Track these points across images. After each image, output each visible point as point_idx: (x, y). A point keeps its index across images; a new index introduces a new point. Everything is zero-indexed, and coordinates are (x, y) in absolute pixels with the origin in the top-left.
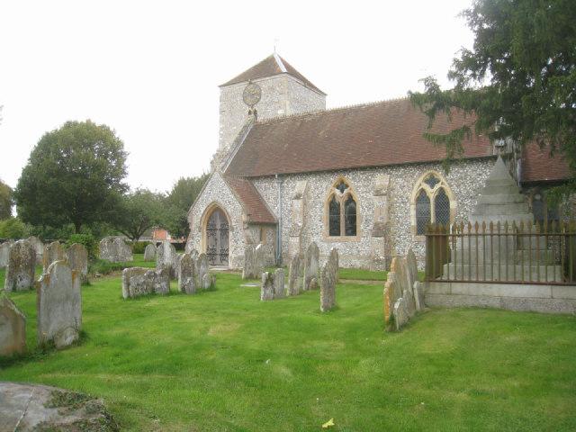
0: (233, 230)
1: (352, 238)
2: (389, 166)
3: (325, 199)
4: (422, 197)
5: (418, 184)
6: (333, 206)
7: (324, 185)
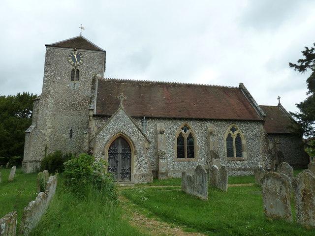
0: (136, 153)
1: (193, 159)
2: (249, 121)
3: (176, 135)
4: (229, 138)
5: (227, 131)
6: (180, 139)
7: (175, 126)
